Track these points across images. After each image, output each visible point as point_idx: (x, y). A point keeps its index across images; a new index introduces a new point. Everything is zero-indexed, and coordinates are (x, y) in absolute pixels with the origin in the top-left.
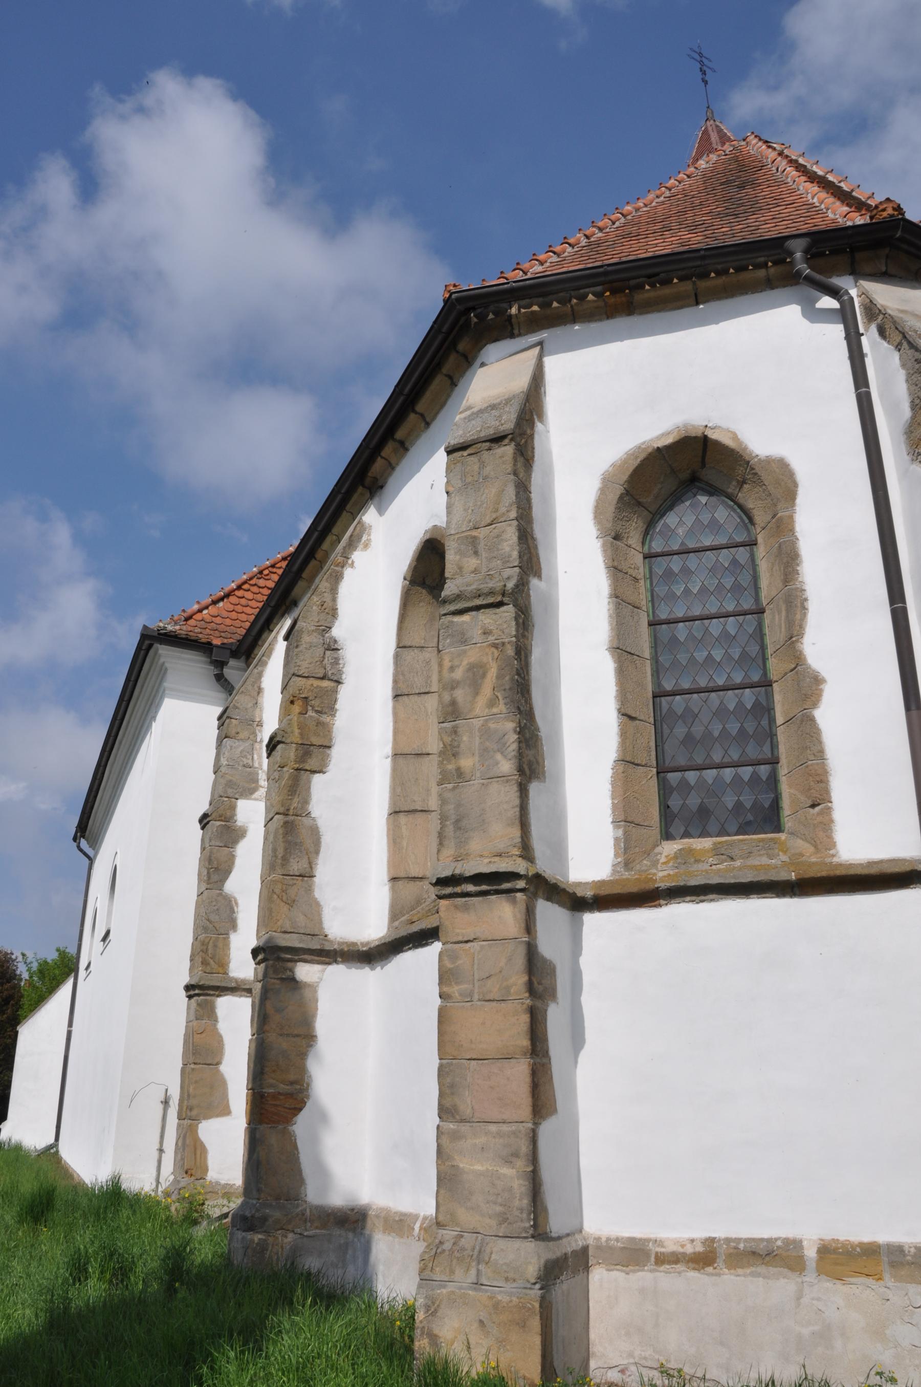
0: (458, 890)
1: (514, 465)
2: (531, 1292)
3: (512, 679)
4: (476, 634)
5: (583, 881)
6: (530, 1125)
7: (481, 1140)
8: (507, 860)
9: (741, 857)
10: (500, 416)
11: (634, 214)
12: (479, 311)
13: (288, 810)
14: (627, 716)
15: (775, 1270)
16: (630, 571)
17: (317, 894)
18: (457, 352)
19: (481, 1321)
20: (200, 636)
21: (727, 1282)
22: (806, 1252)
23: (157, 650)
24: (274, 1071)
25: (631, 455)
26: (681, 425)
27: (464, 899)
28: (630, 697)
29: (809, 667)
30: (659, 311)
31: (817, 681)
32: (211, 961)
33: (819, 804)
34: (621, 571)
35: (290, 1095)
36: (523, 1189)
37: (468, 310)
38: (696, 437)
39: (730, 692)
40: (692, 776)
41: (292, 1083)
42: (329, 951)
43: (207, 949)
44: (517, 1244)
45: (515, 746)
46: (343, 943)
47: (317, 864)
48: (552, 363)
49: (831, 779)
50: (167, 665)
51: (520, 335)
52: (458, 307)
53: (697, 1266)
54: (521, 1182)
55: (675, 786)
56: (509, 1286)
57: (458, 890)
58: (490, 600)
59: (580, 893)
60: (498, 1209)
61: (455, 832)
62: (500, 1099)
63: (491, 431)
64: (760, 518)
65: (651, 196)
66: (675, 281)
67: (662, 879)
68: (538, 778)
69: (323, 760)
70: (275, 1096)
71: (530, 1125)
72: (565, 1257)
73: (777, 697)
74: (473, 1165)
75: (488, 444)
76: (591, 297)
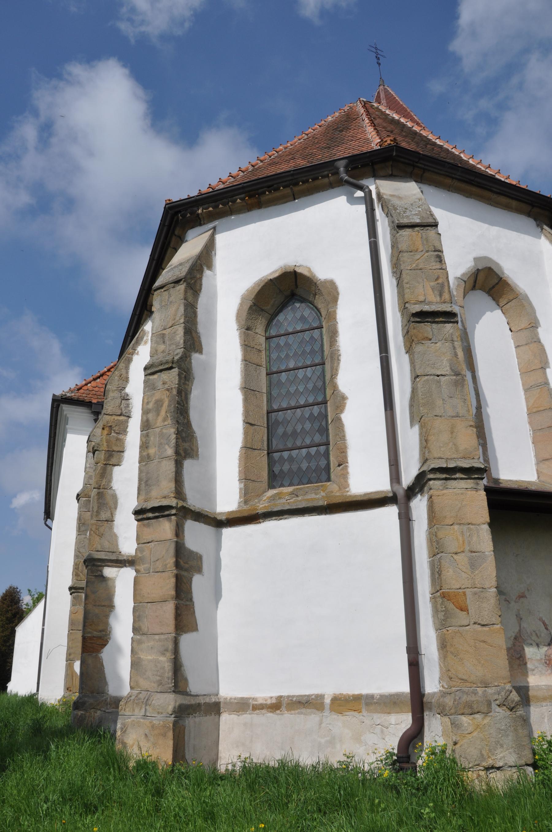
0: (145, 516)
1: (185, 295)
2: (170, 719)
3: (175, 407)
4: (159, 385)
5: (223, 512)
6: (174, 635)
7: (151, 644)
8: (168, 499)
9: (302, 495)
10: (182, 269)
11: (284, 150)
12: (183, 212)
13: (100, 486)
14: (249, 424)
15: (310, 710)
16: (255, 347)
17: (115, 530)
18: (175, 235)
19: (146, 735)
20: (86, 398)
21: (287, 718)
22: (325, 701)
23: (62, 407)
24: (91, 625)
25: (257, 284)
26: (283, 266)
27: (148, 521)
28: (251, 413)
29: (340, 391)
30: (275, 205)
31: (344, 398)
32: (81, 574)
33: (342, 465)
34: (250, 347)
35: (100, 638)
36: (170, 668)
37: (177, 213)
38: (290, 272)
39: (307, 408)
40: (286, 454)
41: (101, 631)
42: (121, 561)
43: (78, 567)
44: (166, 695)
45: (174, 441)
46: (129, 556)
47: (115, 514)
48: (221, 239)
49: (348, 450)
50: (68, 415)
51: (204, 224)
52: (170, 212)
53: (272, 710)
54: (169, 664)
55: (277, 460)
56: (159, 716)
57: (145, 516)
58: (167, 366)
59: (219, 518)
60: (158, 678)
61: (145, 487)
62: (160, 622)
63: (175, 278)
64: (324, 313)
65: (296, 139)
66: (281, 188)
67: (261, 509)
68: (192, 457)
69: (119, 459)
70: (91, 638)
71: (174, 635)
72: (199, 705)
73: (329, 409)
74: (147, 657)
75: (173, 284)
76: (239, 201)
